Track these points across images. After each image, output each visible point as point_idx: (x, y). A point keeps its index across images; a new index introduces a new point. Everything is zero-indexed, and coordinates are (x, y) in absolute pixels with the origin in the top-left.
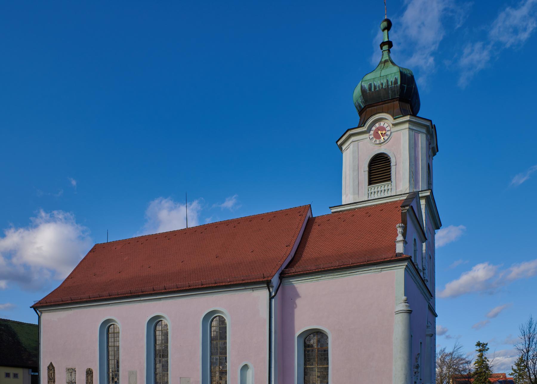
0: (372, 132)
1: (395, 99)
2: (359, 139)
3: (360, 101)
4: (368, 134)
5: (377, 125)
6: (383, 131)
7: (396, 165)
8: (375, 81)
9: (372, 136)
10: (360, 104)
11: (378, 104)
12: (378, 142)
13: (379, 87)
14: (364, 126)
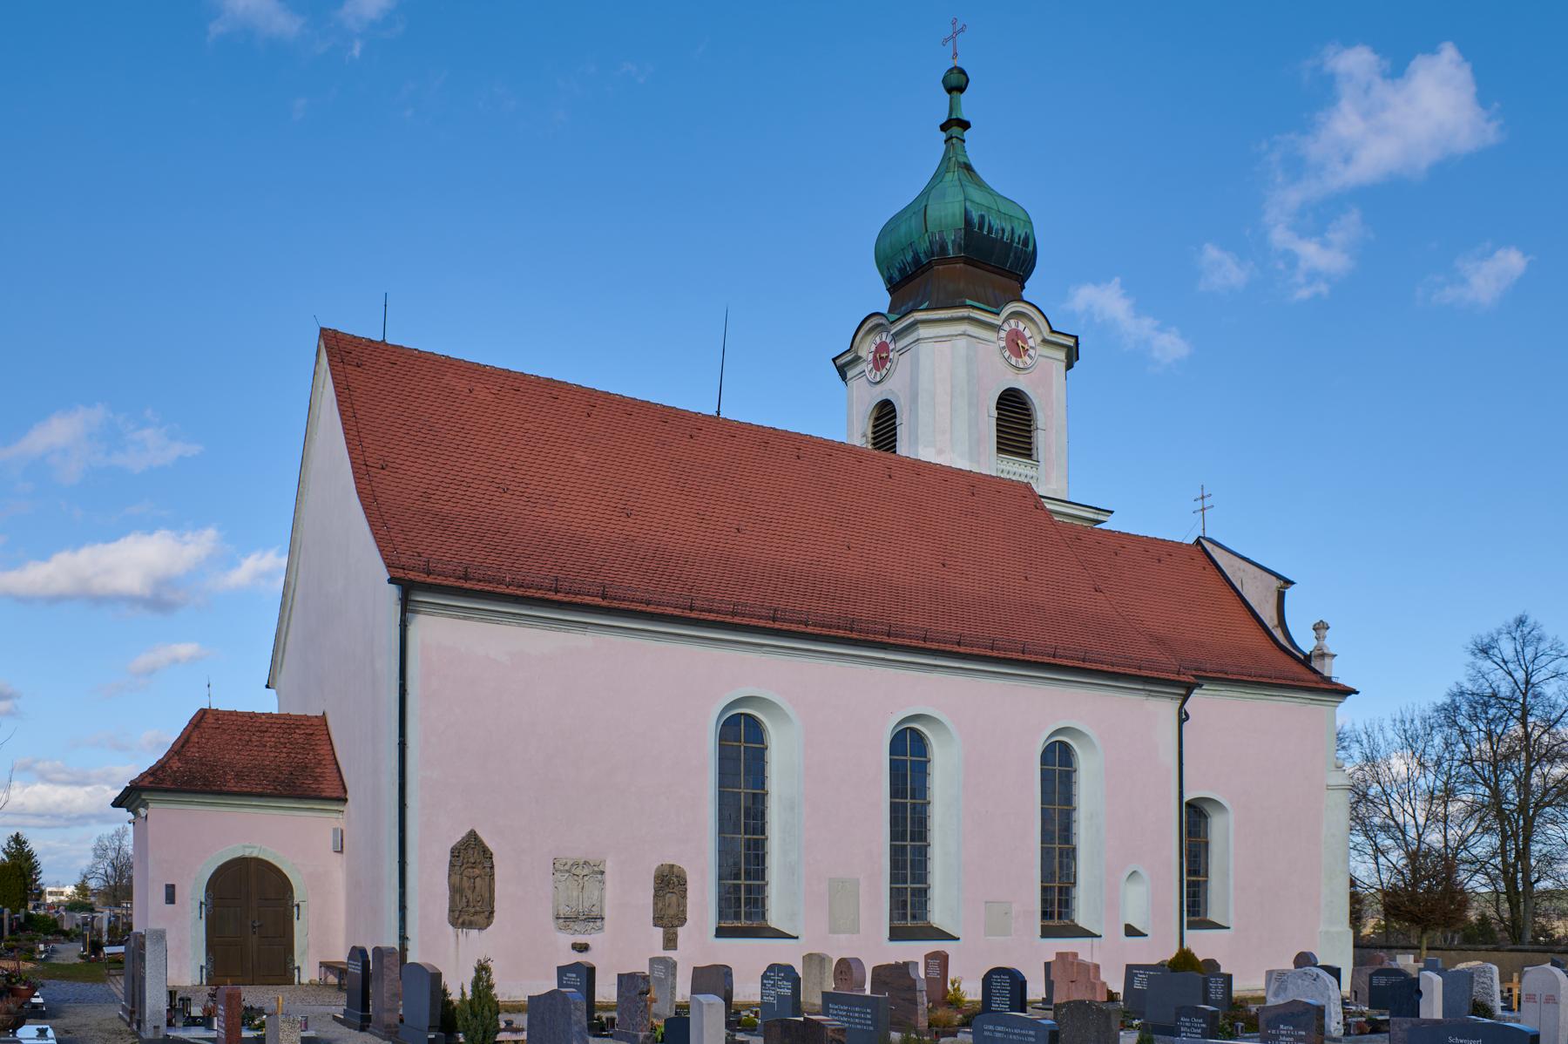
2: (981, 336)
3: (950, 238)
10: (947, 243)
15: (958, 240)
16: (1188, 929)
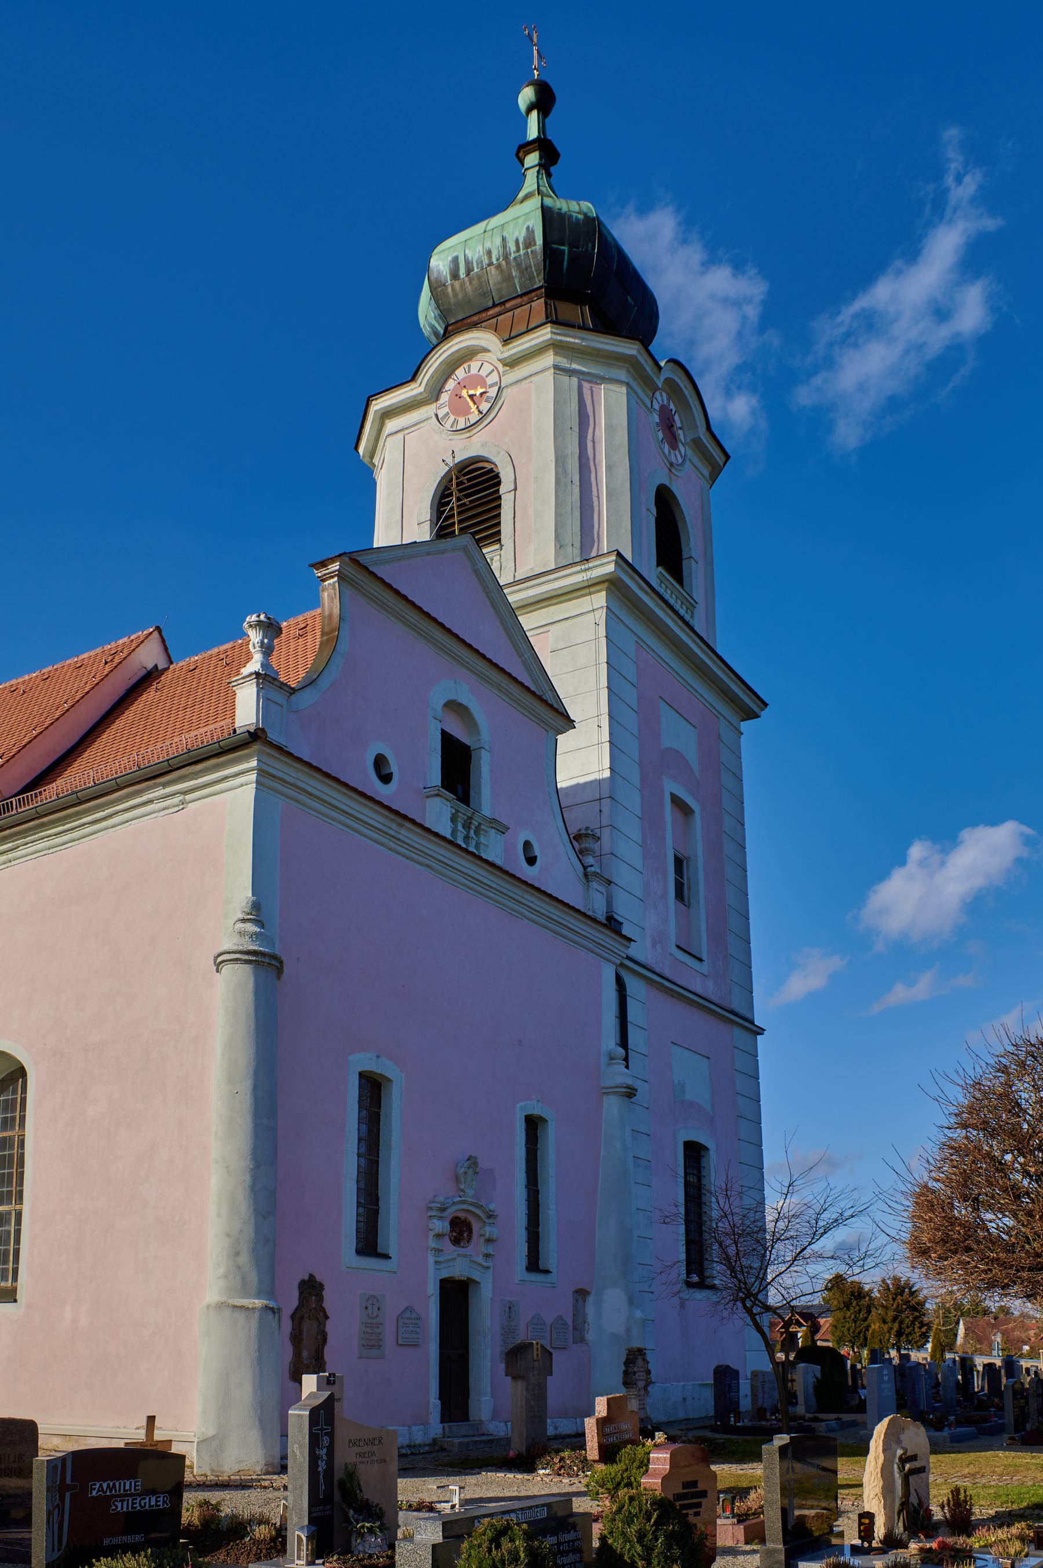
0: (445, 397)
1: (533, 294)
4: (434, 406)
5: (460, 373)
6: (475, 388)
7: (515, 489)
8: (469, 248)
9: (446, 409)
10: (434, 326)
11: (484, 315)
12: (461, 425)
13: (482, 262)
14: (413, 378)
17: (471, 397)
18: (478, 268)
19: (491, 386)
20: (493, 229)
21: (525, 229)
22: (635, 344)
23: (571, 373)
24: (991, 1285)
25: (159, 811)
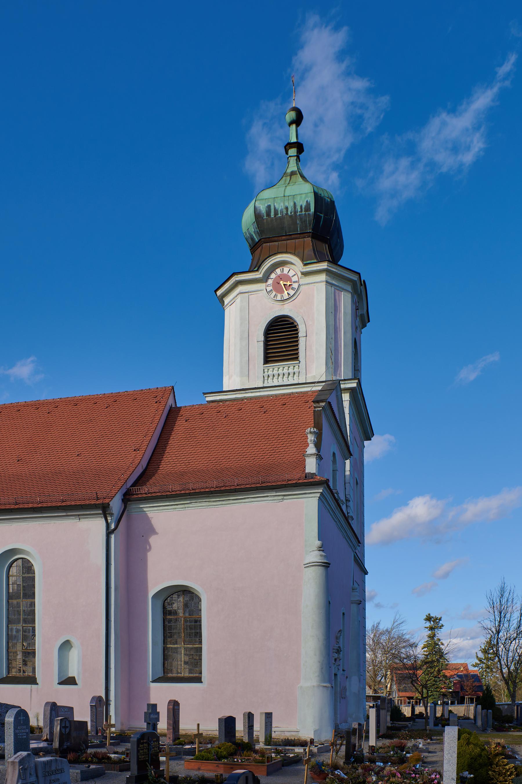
0: (270, 282)
4: (264, 284)
5: (278, 271)
7: (306, 336)
8: (277, 203)
10: (252, 235)
11: (280, 238)
12: (279, 298)
13: (283, 212)
14: (257, 270)
15: (256, 230)
16: (86, 722)
17: (284, 285)
18: (280, 214)
19: (294, 282)
20: (289, 196)
21: (306, 202)
22: (357, 275)
23: (332, 285)
24: (26, 619)
25: (270, 501)
